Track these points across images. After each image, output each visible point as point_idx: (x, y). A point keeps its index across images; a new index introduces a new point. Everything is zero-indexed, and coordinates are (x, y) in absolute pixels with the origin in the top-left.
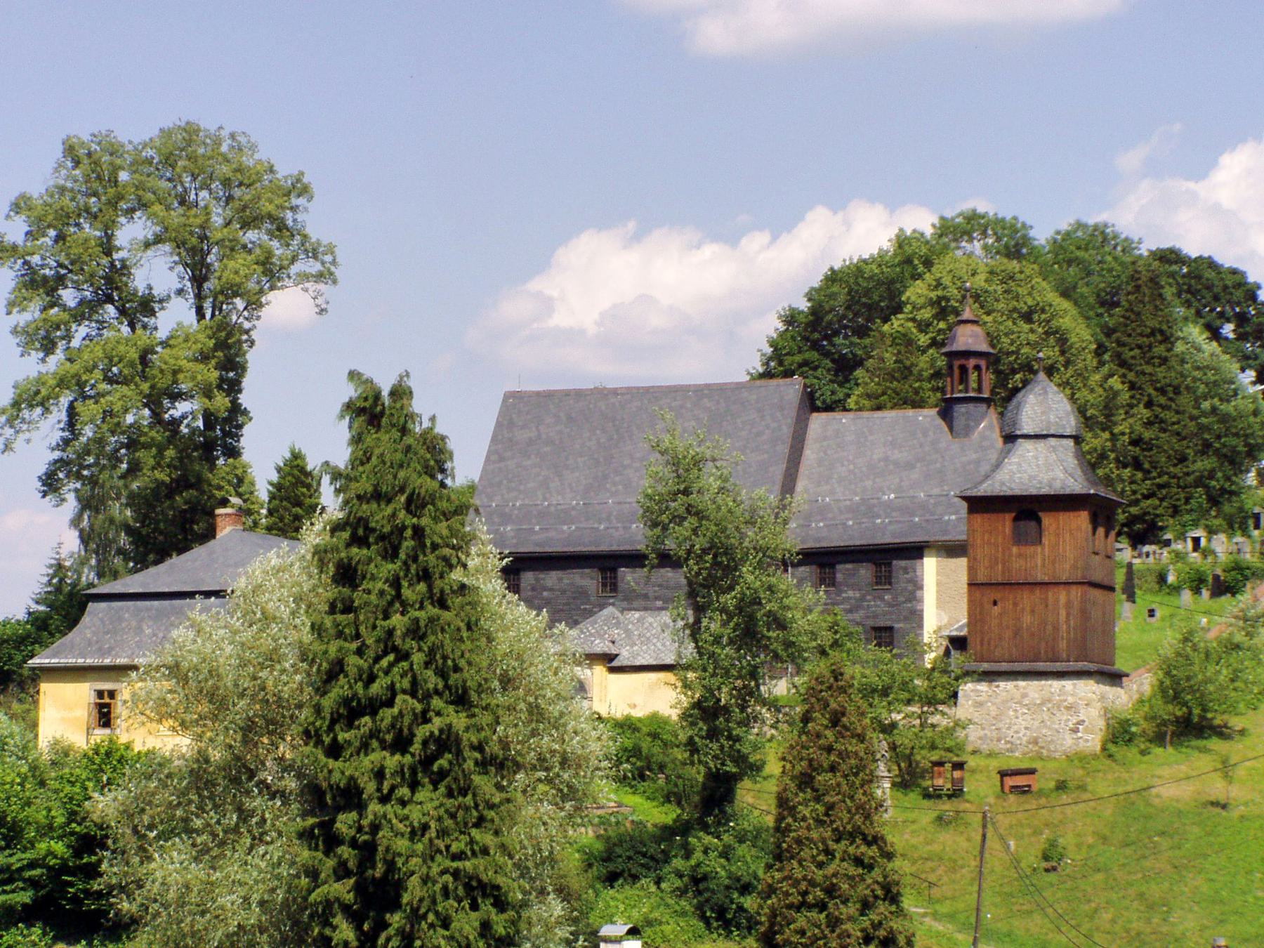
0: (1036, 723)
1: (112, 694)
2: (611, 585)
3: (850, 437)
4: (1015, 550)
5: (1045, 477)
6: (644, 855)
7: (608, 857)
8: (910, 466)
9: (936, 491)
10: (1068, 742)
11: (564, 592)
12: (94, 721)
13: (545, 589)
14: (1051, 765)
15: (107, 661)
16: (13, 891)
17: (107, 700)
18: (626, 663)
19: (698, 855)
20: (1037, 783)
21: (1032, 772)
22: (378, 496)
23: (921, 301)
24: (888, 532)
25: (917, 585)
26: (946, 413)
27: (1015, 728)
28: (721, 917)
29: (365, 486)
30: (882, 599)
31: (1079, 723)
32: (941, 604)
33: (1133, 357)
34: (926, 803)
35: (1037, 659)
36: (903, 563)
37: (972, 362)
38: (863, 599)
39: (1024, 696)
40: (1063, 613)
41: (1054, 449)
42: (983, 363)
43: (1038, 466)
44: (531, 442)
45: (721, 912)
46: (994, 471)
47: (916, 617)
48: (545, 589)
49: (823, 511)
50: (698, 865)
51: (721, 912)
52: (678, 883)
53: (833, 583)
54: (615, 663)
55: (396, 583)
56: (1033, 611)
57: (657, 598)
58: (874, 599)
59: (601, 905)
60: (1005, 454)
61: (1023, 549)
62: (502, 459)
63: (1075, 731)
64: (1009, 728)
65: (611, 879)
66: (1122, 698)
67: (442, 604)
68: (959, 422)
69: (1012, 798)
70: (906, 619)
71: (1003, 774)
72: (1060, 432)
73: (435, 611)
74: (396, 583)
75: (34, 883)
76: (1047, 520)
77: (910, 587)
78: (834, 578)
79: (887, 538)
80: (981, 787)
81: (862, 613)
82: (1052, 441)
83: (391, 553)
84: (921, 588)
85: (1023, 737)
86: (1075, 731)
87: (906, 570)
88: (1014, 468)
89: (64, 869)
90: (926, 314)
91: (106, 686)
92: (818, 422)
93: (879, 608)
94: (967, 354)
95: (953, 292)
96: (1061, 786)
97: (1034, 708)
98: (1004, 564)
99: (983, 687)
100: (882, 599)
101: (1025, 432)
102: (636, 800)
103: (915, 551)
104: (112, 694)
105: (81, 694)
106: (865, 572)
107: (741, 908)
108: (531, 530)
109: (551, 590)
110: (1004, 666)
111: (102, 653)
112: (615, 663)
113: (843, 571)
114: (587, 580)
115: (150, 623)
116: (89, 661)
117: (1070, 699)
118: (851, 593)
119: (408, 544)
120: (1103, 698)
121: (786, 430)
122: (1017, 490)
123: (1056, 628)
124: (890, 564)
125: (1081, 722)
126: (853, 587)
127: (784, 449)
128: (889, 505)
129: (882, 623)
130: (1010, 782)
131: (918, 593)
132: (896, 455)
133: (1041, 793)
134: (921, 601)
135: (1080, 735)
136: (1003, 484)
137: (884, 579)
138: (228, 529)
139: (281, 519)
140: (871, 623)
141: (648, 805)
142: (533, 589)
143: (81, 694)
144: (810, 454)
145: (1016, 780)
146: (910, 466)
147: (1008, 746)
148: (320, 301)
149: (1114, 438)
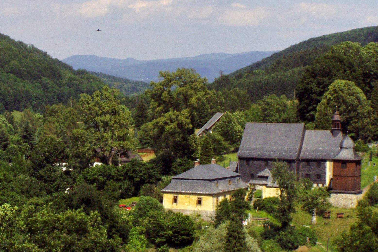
1: (177, 197)
2: (267, 165)
3: (313, 136)
4: (341, 170)
5: (347, 156)
6: (271, 234)
7: (265, 234)
8: (324, 142)
9: (329, 148)
10: (350, 206)
14: (347, 211)
15: (176, 191)
16: (163, 239)
18: (269, 186)
19: (281, 236)
20: (344, 216)
21: (342, 214)
22: (233, 231)
23: (332, 90)
24: (320, 156)
25: (325, 167)
26: (332, 131)
28: (284, 247)
29: (231, 230)
32: (330, 171)
33: (375, 102)
34: (323, 219)
35: (345, 190)
36: (323, 162)
37: (337, 122)
39: (343, 197)
41: (349, 151)
42: (339, 123)
44: (252, 134)
45: (285, 246)
46: (338, 154)
47: (325, 173)
49: (308, 151)
50: (281, 237)
51: (285, 246)
52: (277, 240)
53: (309, 165)
54: (267, 186)
55: (236, 244)
59: (264, 244)
60: (340, 151)
63: (352, 204)
65: (266, 238)
66: (361, 197)
67: (242, 246)
68: (334, 134)
69: (339, 219)
70: (323, 173)
71: (338, 214)
73: (241, 247)
74: (236, 244)
75: (166, 237)
76: (348, 164)
79: (320, 158)
80: (333, 215)
82: (349, 149)
83: (235, 239)
86: (352, 204)
87: (323, 164)
89: (172, 236)
90: (332, 93)
91: (176, 195)
93: (318, 171)
94: (336, 121)
95: (338, 89)
96: (348, 217)
97: (345, 199)
99: (335, 195)
102: (270, 217)
103: (325, 160)
104: (177, 197)
105: (171, 196)
106: (315, 164)
107: (288, 246)
108: (252, 152)
110: (339, 191)
111: (175, 189)
112: (267, 186)
113: (311, 163)
114: (262, 163)
116: (173, 191)
119: (237, 239)
120: (357, 197)
122: (342, 159)
124: (320, 163)
125: (353, 202)
127: (300, 138)
128: (321, 151)
129: (318, 174)
130: (339, 216)
132: (322, 140)
133: (344, 218)
137: (319, 165)
138: (197, 165)
139: (204, 151)
140: (317, 173)
141: (273, 218)
143: (171, 196)
144: (306, 139)
145: (340, 215)
146: (324, 142)
149: (371, 120)
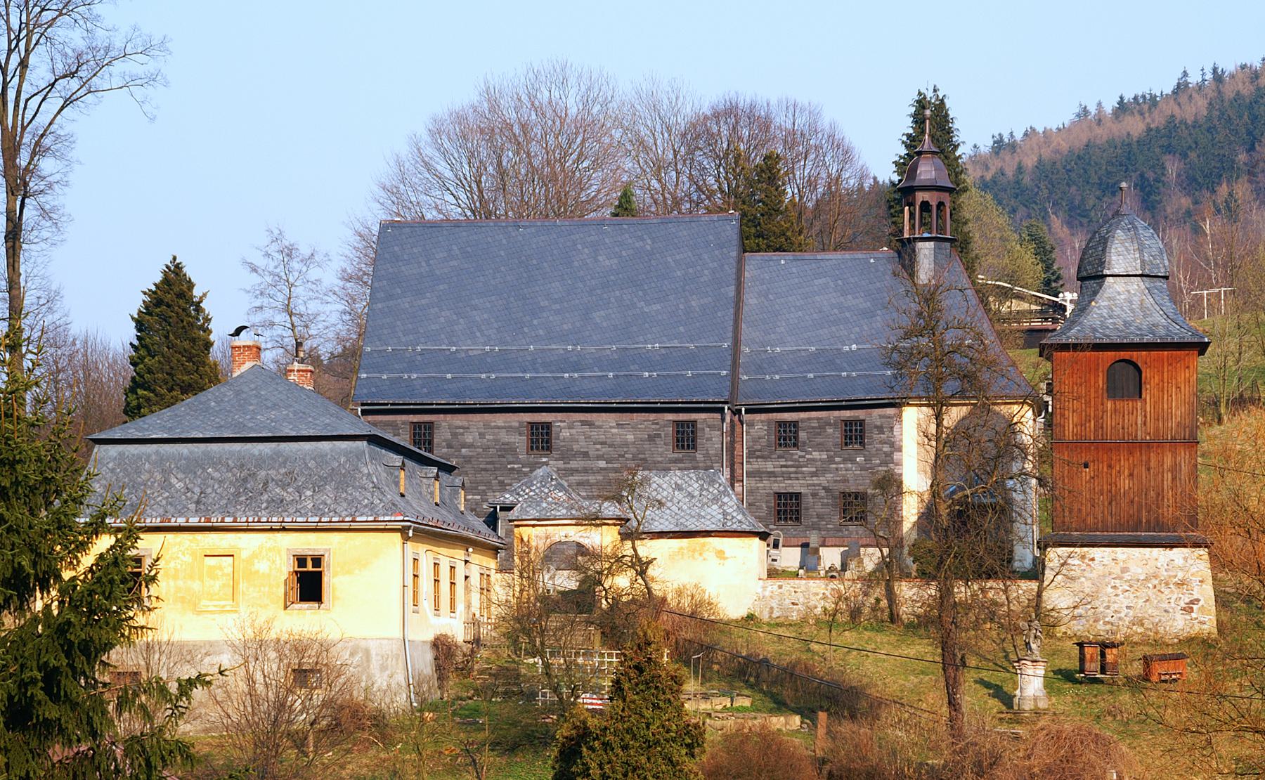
0: (1141, 602)
4: (1109, 405)
11: (486, 448)
12: (295, 594)
13: (464, 446)
17: (310, 568)
27: (1115, 607)
30: (853, 461)
31: (1192, 602)
38: (831, 460)
40: (1168, 476)
43: (1132, 311)
48: (464, 446)
56: (1131, 475)
57: (599, 458)
58: (845, 461)
61: (1119, 404)
62: (390, 297)
64: (1108, 607)
72: (1155, 272)
77: (886, 449)
78: (796, 438)
81: (829, 476)
84: (900, 450)
85: (1127, 616)
88: (1105, 312)
92: (754, 262)
98: (1096, 422)
100: (853, 461)
101: (1116, 271)
109: (470, 446)
115: (180, 476)
117: (1180, 575)
118: (816, 455)
121: (730, 271)
123: (1160, 494)
126: (820, 447)
131: (896, 456)
134: (899, 464)
135: (1194, 615)
136: (1094, 330)
142: (449, 446)
147: (1108, 627)
148: (147, 108)
